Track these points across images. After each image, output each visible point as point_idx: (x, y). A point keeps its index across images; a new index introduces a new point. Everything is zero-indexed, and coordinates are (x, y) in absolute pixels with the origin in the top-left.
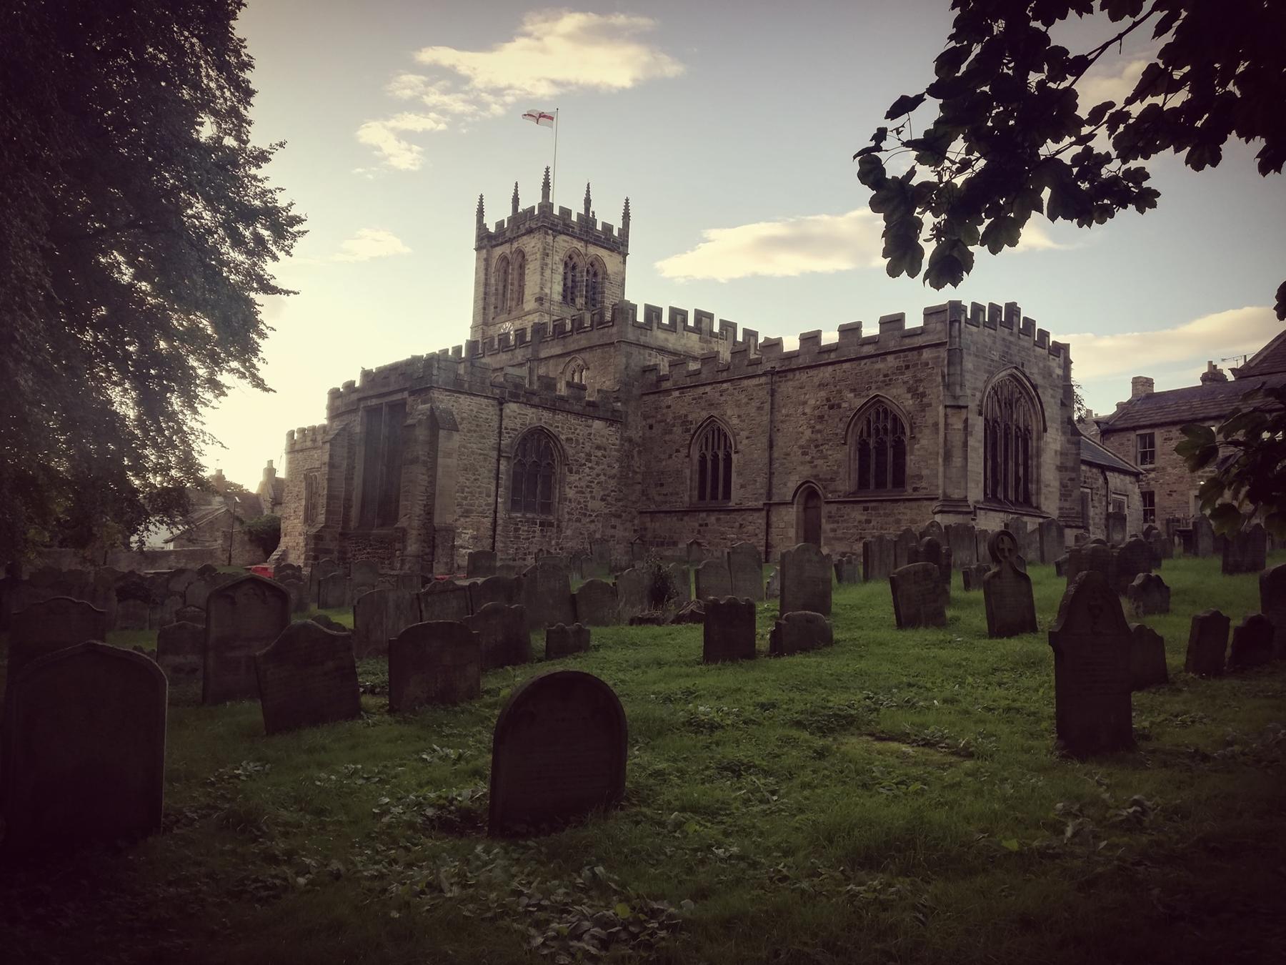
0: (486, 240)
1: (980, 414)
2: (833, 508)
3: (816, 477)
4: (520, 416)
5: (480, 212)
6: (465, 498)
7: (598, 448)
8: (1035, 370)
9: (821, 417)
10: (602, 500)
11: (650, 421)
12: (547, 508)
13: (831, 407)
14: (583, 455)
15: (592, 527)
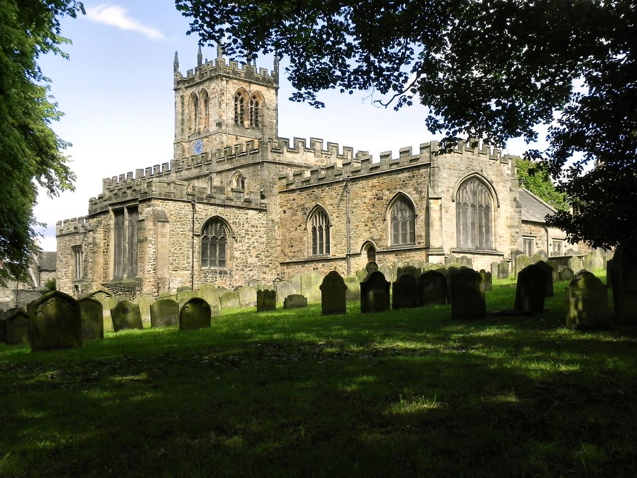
0: (181, 83)
3: (372, 238)
4: (206, 212)
5: (176, 65)
6: (175, 260)
7: (253, 226)
8: (491, 173)
10: (257, 257)
11: (284, 208)
12: (222, 263)
14: (243, 231)
15: (251, 273)
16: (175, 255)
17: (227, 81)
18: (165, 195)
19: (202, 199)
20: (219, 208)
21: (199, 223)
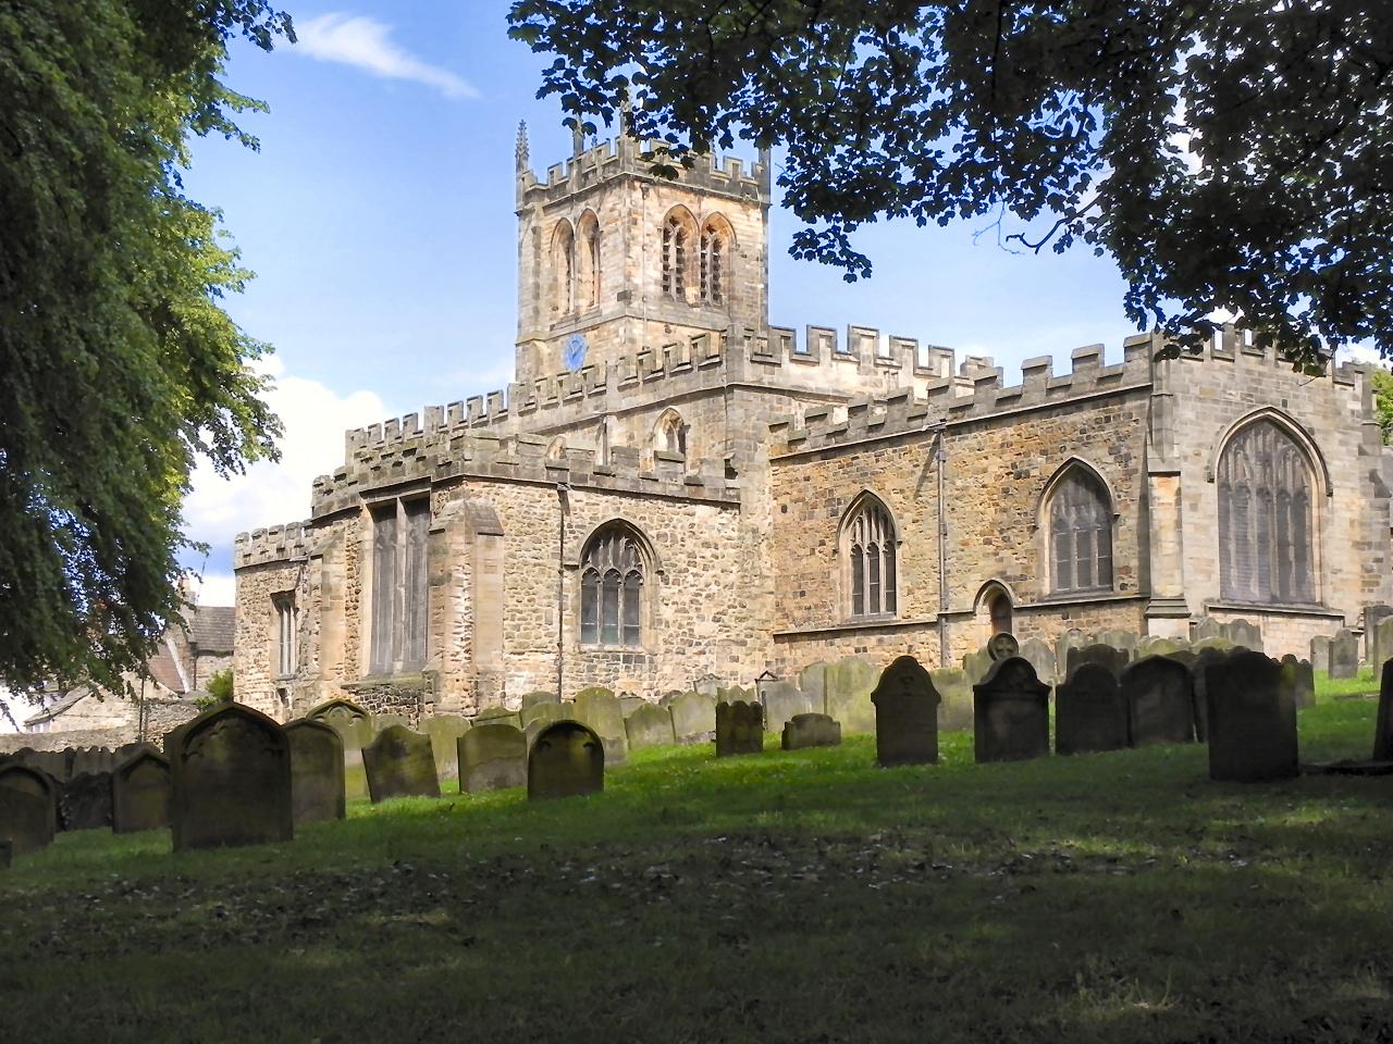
1: (1212, 481)
2: (1026, 619)
7: (706, 545)
9: (1006, 491)
10: (716, 620)
13: (1018, 477)
14: (684, 557)
15: (702, 660)
16: (518, 615)
17: (645, 192)
18: (494, 470)
19: (584, 478)
20: (623, 500)
21: (575, 538)
